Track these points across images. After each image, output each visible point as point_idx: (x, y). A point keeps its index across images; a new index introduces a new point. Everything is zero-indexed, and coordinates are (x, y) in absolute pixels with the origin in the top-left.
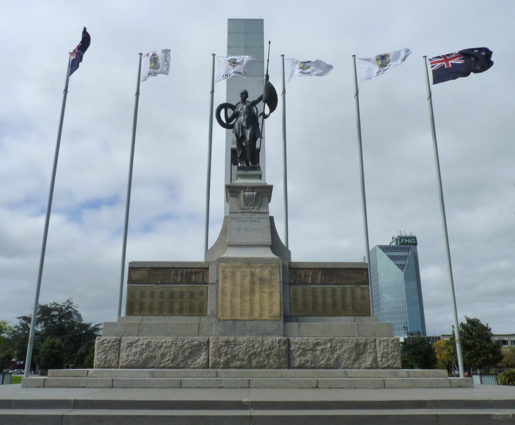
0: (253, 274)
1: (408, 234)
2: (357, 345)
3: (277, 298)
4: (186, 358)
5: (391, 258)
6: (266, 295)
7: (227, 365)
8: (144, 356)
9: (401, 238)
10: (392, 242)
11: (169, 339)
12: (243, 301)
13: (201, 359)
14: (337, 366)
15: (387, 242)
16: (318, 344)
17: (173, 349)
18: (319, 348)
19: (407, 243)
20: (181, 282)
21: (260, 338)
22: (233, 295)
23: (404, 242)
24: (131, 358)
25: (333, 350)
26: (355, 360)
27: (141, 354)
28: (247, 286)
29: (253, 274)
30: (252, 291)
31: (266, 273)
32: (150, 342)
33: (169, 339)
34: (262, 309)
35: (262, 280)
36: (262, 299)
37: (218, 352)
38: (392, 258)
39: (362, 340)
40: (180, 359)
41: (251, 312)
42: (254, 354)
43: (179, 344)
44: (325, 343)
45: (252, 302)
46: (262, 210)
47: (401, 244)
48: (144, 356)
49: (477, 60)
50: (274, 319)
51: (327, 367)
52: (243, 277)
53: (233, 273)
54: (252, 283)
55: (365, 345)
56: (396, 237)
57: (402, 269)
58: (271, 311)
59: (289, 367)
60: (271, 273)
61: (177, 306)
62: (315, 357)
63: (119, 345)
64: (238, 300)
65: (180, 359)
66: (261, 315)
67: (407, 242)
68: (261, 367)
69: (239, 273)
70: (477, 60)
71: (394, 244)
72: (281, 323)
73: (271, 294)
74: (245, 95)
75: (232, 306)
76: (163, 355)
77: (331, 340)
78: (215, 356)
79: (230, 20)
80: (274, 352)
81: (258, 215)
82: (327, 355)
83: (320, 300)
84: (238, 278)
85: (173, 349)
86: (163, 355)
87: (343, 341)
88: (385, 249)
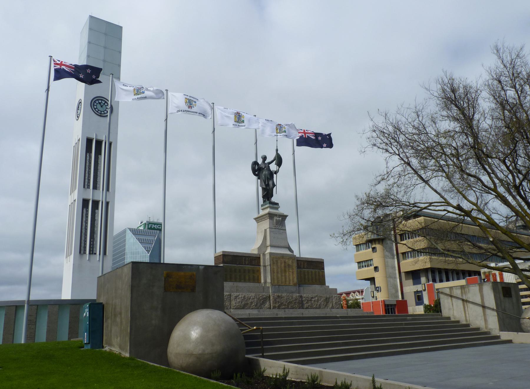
0: (285, 262)
1: (155, 221)
2: (326, 298)
3: (295, 275)
4: (261, 304)
5: (139, 241)
6: (291, 273)
7: (279, 308)
8: (243, 303)
9: (149, 223)
10: (140, 226)
11: (253, 295)
12: (282, 276)
13: (267, 305)
14: (319, 308)
15: (136, 224)
16: (312, 298)
17: (255, 299)
18: (313, 300)
19: (154, 229)
20: (248, 265)
21: (291, 295)
22: (277, 272)
23: (151, 227)
24: (237, 304)
25: (318, 301)
26: (326, 305)
27: (242, 302)
28: (283, 268)
29: (285, 262)
30: (285, 271)
31: (290, 262)
32: (245, 296)
33: (253, 295)
34: (290, 280)
35: (289, 265)
36: (289, 276)
37: (275, 301)
38: (141, 242)
39: (328, 297)
40: (259, 305)
41: (286, 281)
42: (289, 302)
43: (258, 296)
44: (315, 297)
45: (285, 276)
46: (283, 228)
47: (149, 229)
48: (243, 303)
49: (322, 141)
50: (295, 285)
51: (316, 308)
52: (281, 263)
53: (277, 261)
54: (285, 267)
55: (329, 298)
56: (145, 222)
57: (148, 251)
58: (293, 281)
59: (303, 308)
60: (292, 263)
61: (247, 278)
62: (312, 304)
63: (230, 297)
64: (280, 276)
65: (259, 305)
66: (289, 283)
67: (154, 228)
68: (292, 308)
69: (279, 261)
70: (322, 141)
71: (142, 228)
72: (297, 287)
73: (293, 272)
74: (264, 158)
75: (278, 278)
76: (252, 303)
77: (317, 296)
78: (274, 303)
79: (91, 17)
80: (297, 301)
81: (282, 231)
82: (316, 303)
83: (307, 277)
84: (279, 264)
85: (255, 299)
86: (252, 303)
87: (321, 297)
88: (135, 232)
